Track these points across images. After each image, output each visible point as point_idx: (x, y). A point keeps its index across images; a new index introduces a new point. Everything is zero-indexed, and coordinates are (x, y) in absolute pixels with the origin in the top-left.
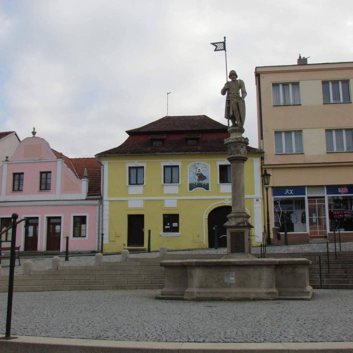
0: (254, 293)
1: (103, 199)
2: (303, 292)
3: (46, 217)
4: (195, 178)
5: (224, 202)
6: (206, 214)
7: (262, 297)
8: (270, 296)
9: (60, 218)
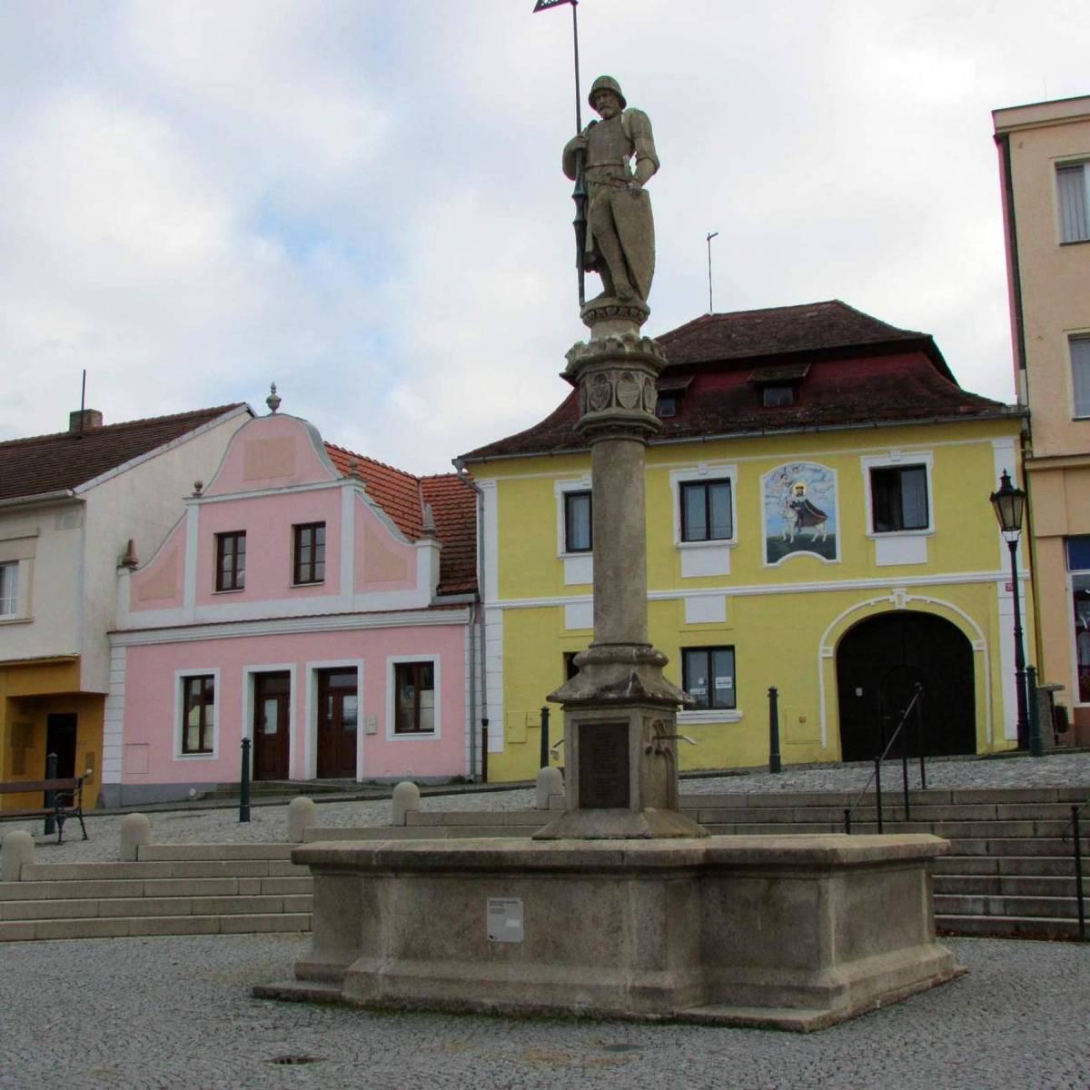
0: (591, 990)
1: (483, 603)
2: (802, 990)
3: (247, 674)
4: (785, 518)
5: (892, 599)
6: (826, 643)
7: (617, 1007)
8: (648, 1004)
9: (352, 670)
